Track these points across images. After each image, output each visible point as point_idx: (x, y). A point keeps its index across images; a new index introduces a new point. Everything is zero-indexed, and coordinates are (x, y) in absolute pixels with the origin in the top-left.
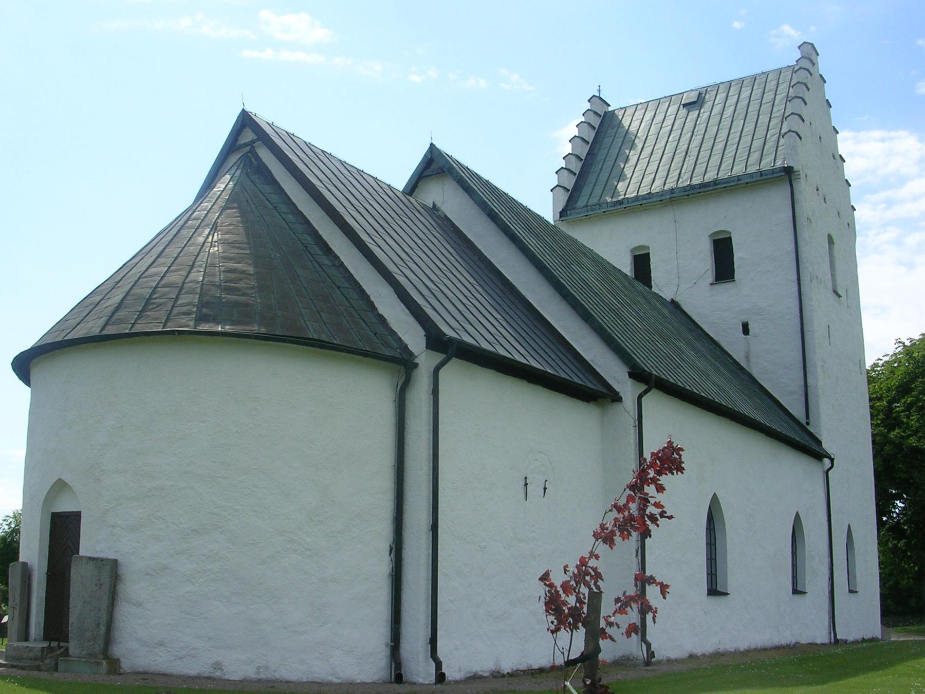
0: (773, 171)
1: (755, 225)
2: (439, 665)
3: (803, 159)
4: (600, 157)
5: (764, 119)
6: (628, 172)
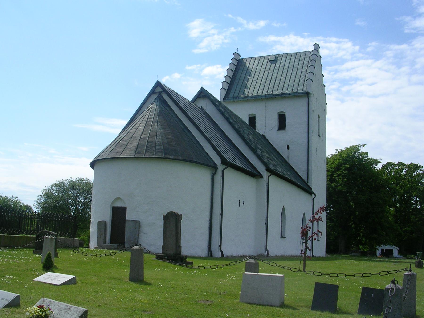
0: (302, 93)
1: (294, 111)
2: (222, 252)
3: (313, 89)
4: (238, 77)
5: (299, 71)
6: (249, 85)
